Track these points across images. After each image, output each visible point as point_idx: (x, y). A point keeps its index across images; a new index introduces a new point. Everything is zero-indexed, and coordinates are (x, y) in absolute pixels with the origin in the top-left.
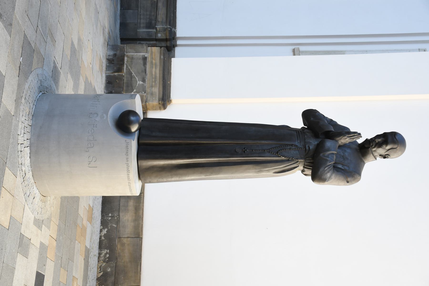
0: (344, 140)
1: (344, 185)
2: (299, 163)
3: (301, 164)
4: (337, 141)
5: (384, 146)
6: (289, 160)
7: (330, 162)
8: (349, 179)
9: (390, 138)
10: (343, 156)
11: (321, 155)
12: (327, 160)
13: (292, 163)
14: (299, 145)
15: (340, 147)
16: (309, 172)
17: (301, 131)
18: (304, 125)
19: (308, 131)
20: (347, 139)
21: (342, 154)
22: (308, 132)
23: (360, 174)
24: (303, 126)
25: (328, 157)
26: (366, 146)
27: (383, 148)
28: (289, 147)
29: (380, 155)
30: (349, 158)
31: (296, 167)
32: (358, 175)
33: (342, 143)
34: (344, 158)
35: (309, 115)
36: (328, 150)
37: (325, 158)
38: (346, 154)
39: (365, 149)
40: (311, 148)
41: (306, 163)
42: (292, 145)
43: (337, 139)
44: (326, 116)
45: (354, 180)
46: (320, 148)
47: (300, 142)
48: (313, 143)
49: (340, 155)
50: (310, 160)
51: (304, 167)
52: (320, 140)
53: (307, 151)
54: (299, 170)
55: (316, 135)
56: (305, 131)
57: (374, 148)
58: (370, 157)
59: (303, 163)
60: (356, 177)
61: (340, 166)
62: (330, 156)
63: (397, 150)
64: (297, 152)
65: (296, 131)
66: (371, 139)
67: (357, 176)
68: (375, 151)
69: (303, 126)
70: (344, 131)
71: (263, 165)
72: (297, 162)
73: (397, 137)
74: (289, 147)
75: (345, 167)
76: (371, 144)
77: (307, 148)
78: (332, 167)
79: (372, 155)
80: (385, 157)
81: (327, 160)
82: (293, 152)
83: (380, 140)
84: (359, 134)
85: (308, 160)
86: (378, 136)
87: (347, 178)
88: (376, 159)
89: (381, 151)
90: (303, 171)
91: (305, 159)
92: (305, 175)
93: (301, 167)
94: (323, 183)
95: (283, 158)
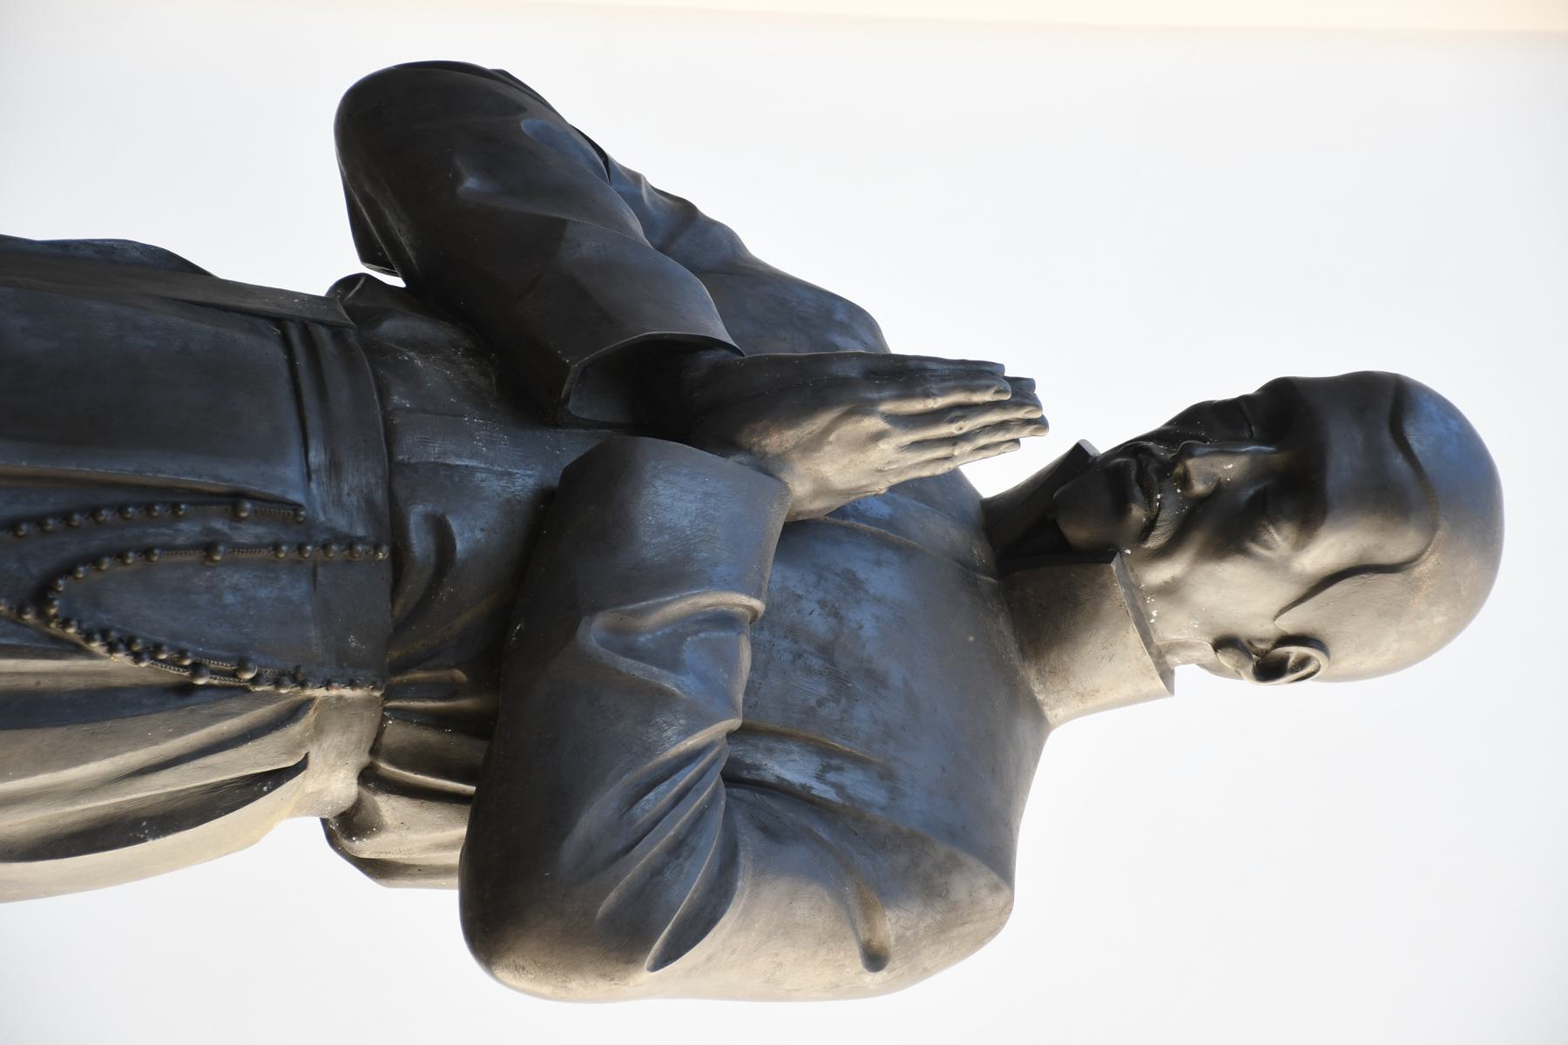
0: (849, 460)
1: (837, 991)
2: (319, 731)
3: (335, 739)
4: (769, 468)
5: (1279, 539)
6: (184, 690)
7: (700, 719)
8: (890, 926)
9: (1344, 455)
10: (826, 651)
11: (594, 632)
12: (655, 699)
14: (315, 499)
15: (798, 531)
16: (436, 835)
17: (337, 331)
18: (367, 251)
19: (421, 327)
20: (886, 448)
21: (819, 624)
22: (424, 348)
23: (998, 861)
24: (353, 264)
25: (673, 664)
26: (1078, 533)
27: (1269, 565)
28: (189, 530)
30: (895, 672)
31: (277, 778)
32: (984, 878)
33: (823, 490)
34: (837, 665)
35: (429, 141)
37: (626, 664)
38: (865, 620)
39: (1058, 552)
40: (468, 536)
41: (396, 734)
42: (233, 500)
43: (778, 440)
44: (622, 154)
45: (941, 930)
47: (334, 467)
48: (490, 479)
49: (793, 632)
50: (452, 691)
51: (368, 777)
52: (569, 448)
53: (415, 585)
54: (301, 809)
55: (522, 390)
56: (389, 327)
57: (1164, 553)
58: (1108, 659)
59: (362, 730)
60: (960, 887)
61: (790, 768)
62: (690, 652)
63: (1414, 588)
64: (298, 590)
65: (278, 321)
66: (1133, 449)
67: (969, 883)
68: (1169, 591)
69: (353, 264)
70: (815, 357)
71: (427, 803)
72: (295, 712)
73: (1417, 438)
74: (189, 530)
75: (856, 782)
76: (1138, 513)
77: (420, 543)
78: (714, 779)
79: (1134, 636)
80: (1269, 669)
81: (655, 699)
82: (246, 592)
83: (1230, 467)
84: (1022, 391)
85: (423, 690)
86: (1204, 424)
87: (868, 910)
88: (1166, 675)
89: (1242, 591)
90: (346, 827)
91: (389, 670)
92: (377, 869)
93: (333, 780)
94: (603, 986)
95: (121, 660)
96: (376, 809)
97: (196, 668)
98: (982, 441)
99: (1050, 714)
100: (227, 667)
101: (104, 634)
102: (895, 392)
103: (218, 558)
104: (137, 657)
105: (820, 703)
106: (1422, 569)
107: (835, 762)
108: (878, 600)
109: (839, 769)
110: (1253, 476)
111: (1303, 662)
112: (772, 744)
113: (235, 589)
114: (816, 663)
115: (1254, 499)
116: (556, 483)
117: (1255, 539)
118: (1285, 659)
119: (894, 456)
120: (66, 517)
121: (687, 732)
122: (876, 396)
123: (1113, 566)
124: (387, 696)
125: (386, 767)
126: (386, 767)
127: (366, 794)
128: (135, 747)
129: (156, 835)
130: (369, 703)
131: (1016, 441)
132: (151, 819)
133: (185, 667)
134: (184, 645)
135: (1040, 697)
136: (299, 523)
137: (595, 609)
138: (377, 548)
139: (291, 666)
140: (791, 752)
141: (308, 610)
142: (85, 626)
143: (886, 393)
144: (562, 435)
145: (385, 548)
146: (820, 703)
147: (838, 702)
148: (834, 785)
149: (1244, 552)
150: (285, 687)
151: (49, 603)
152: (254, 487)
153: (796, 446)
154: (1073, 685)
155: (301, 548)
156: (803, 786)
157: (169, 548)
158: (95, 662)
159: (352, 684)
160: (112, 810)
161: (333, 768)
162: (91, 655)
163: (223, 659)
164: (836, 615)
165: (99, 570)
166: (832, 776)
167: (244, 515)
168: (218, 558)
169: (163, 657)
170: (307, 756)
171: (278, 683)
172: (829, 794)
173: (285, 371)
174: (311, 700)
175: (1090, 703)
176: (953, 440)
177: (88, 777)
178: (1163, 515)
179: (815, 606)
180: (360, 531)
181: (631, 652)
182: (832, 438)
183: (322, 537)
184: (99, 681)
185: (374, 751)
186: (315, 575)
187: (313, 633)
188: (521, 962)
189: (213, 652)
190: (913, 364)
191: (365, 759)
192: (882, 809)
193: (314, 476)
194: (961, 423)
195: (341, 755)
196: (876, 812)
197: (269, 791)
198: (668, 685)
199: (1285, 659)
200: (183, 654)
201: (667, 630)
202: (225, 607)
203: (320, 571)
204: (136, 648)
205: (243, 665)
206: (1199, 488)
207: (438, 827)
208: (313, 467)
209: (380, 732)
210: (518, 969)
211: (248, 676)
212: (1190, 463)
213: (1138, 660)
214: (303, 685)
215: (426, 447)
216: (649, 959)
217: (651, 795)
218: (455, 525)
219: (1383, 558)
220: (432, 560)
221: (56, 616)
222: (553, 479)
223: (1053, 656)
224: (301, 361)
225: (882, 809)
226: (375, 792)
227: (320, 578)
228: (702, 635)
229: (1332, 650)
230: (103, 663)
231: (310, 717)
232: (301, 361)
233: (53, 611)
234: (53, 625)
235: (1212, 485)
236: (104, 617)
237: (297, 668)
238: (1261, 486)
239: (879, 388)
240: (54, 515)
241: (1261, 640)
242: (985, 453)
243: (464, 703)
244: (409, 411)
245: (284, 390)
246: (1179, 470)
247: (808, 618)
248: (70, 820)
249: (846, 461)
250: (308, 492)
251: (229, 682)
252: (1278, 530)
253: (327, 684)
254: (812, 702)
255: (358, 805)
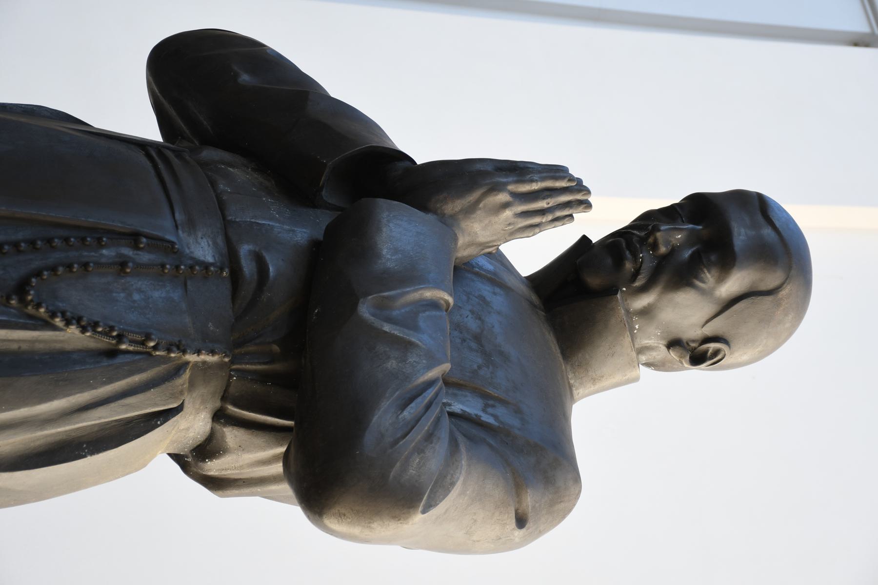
1: (502, 545)
2: (192, 385)
3: (202, 390)
4: (449, 223)
5: (709, 277)
6: (112, 353)
7: (433, 362)
10: (477, 338)
13: (137, 379)
20: (508, 213)
21: (472, 324)
25: (415, 328)
26: (594, 281)
27: (703, 292)
29: (674, 344)
31: (166, 415)
36: (409, 276)
38: (493, 320)
39: (581, 297)
42: (134, 238)
43: (453, 206)
46: (333, 275)
48: (286, 233)
51: (219, 416)
52: (324, 219)
55: (294, 185)
57: (644, 289)
58: (612, 354)
63: (778, 304)
64: (176, 295)
68: (646, 313)
74: (108, 253)
76: (629, 266)
77: (248, 267)
80: (698, 359)
82: (146, 298)
84: (579, 187)
89: (686, 311)
90: (194, 460)
91: (236, 344)
92: (215, 484)
96: (223, 436)
97: (120, 338)
98: (559, 214)
99: (575, 392)
100: (139, 338)
101: (63, 314)
102: (515, 179)
103: (128, 270)
104: (84, 330)
105: (479, 367)
106: (783, 293)
107: (491, 402)
108: (499, 313)
109: (493, 406)
110: (689, 242)
111: (716, 352)
112: (456, 391)
113: (139, 291)
114: (474, 345)
115: (692, 256)
116: (321, 238)
117: (697, 277)
118: (706, 351)
119: (513, 220)
120: (32, 243)
121: (429, 368)
122: (504, 180)
123: (619, 296)
124: (232, 362)
125: (232, 409)
126: (232, 409)
127: (218, 427)
128: (82, 391)
129: (92, 453)
130: (220, 366)
131: (571, 216)
132: (89, 443)
133: (113, 337)
134: (112, 323)
135: (572, 382)
136: (175, 253)
137: (367, 294)
138: (222, 269)
139: (176, 340)
140: (466, 396)
141: (184, 306)
142: (50, 308)
143: (510, 179)
144: (318, 211)
145: (227, 270)
146: (479, 367)
147: (488, 367)
148: (492, 415)
149: (690, 285)
150: (174, 352)
151: (27, 293)
152: (146, 230)
153: (461, 211)
154: (590, 373)
155: (177, 267)
156: (476, 415)
157: (98, 264)
158: (57, 333)
159: (213, 352)
160: (65, 437)
161: (198, 412)
162: (55, 328)
163: (137, 333)
164: (480, 319)
165: (56, 275)
166: (490, 410)
167: (142, 246)
168: (128, 270)
169: (100, 329)
170: (183, 404)
171: (169, 350)
172: (490, 420)
173: (152, 172)
174: (187, 363)
175: (598, 386)
176: (542, 212)
177: (48, 413)
178: (644, 266)
179: (468, 313)
180: (210, 259)
181: (389, 320)
182: (481, 205)
183: (190, 262)
184: (58, 346)
185: (224, 399)
186: (185, 285)
187: (187, 320)
188: (343, 511)
189: (133, 329)
190: (522, 166)
191: (218, 404)
192: (519, 429)
193: (180, 227)
194: (549, 200)
195: (203, 402)
196: (517, 432)
197: (162, 424)
198: (413, 340)
199: (706, 351)
200: (112, 329)
201: (407, 309)
202: (134, 301)
203: (189, 283)
204: (83, 323)
205: (148, 337)
206: (663, 250)
207: (263, 449)
208: (179, 222)
209: (228, 385)
210: (341, 516)
211: (152, 344)
212: (658, 234)
213: (628, 355)
214: (184, 352)
215: (239, 214)
216: (420, 509)
217: (413, 405)
218: (268, 257)
219: (763, 287)
220: (256, 277)
221: (32, 301)
222: (319, 235)
223: (580, 355)
224: (161, 166)
225: (519, 429)
226: (225, 425)
227: (189, 287)
228: (427, 313)
229: (732, 345)
230: (62, 333)
231: (187, 375)
232: (161, 166)
233: (30, 298)
234: (30, 308)
235: (670, 248)
236: (60, 304)
237: (180, 341)
238: (693, 249)
239: (506, 176)
240: (25, 241)
241: (693, 341)
242: (557, 223)
243: (277, 367)
244: (230, 193)
245: (155, 181)
246: (651, 240)
247: (466, 320)
248: (38, 443)
249: (487, 222)
250: (177, 236)
251: (140, 348)
252: (709, 272)
253: (198, 352)
254: (475, 367)
255: (211, 437)
